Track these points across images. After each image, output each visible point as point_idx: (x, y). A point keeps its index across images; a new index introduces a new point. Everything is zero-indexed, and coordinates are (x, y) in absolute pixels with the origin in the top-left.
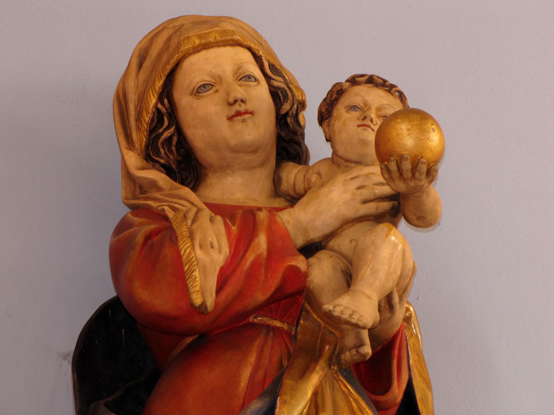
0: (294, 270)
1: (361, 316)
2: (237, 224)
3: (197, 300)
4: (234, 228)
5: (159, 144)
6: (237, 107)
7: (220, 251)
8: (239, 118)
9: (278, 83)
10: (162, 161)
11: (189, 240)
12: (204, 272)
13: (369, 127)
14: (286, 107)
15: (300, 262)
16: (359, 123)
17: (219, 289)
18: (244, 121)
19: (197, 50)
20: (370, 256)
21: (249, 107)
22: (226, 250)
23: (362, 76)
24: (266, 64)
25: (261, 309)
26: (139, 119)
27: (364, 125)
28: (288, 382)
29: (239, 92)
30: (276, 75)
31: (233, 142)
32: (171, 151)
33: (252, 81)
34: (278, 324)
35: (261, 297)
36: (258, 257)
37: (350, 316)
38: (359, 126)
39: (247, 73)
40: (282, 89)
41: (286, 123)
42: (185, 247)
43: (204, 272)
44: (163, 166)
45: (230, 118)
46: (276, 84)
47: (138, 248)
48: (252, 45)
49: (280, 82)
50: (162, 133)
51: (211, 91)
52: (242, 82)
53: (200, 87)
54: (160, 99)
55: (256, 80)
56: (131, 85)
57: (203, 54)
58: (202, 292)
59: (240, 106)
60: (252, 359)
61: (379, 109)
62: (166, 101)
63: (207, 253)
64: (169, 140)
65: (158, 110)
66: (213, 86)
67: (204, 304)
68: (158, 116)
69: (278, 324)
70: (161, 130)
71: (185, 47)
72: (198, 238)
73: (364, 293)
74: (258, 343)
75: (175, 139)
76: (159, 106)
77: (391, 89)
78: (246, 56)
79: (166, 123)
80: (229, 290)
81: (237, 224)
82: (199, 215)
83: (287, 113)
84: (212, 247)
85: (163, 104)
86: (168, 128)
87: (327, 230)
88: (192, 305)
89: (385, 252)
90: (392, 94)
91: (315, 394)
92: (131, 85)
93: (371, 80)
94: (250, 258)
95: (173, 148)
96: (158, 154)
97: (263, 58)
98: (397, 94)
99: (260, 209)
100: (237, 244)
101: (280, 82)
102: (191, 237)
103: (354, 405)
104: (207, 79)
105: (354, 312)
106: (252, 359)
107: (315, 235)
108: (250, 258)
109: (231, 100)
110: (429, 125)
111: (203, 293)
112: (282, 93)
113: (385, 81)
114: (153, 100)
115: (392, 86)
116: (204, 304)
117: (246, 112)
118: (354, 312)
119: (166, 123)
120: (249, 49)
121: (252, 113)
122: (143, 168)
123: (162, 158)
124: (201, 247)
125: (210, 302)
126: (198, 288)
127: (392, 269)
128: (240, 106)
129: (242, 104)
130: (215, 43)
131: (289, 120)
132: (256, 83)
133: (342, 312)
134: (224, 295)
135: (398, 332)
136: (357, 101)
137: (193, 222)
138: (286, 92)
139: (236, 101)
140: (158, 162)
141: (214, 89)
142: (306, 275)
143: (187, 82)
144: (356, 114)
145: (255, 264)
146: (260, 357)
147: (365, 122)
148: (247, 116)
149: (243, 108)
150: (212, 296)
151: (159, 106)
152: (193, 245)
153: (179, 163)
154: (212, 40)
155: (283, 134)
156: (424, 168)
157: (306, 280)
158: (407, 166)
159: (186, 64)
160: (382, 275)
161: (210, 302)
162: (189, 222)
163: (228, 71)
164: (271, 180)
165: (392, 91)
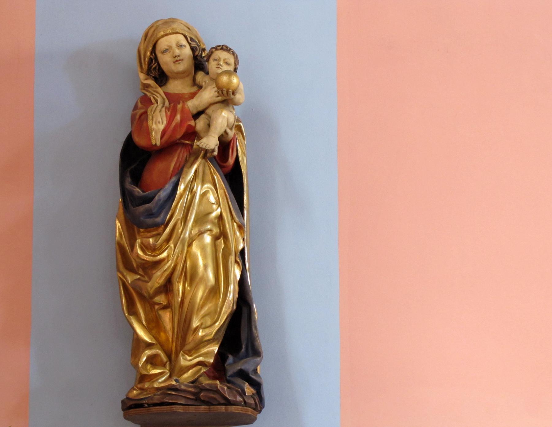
1: (210, 146)
2: (170, 111)
3: (154, 143)
4: (169, 113)
5: (152, 70)
6: (176, 59)
7: (162, 123)
8: (177, 62)
9: (194, 44)
10: (153, 75)
11: (152, 120)
12: (156, 132)
13: (220, 68)
14: (197, 53)
15: (192, 123)
16: (217, 66)
17: (162, 138)
18: (179, 63)
19: (163, 36)
20: (214, 122)
21: (181, 58)
22: (165, 122)
24: (189, 39)
26: (144, 60)
27: (218, 67)
28: (185, 169)
29: (177, 52)
30: (193, 42)
31: (175, 71)
32: (156, 72)
33: (183, 47)
34: (187, 142)
35: (178, 137)
36: (177, 124)
37: (205, 147)
38: (216, 68)
39: (181, 44)
40: (195, 47)
41: (197, 58)
42: (150, 122)
43: (156, 132)
44: (153, 77)
45: (174, 62)
46: (192, 45)
47: (136, 121)
48: (183, 33)
49: (194, 44)
50: (152, 66)
51: (168, 52)
52: (179, 48)
53: (164, 51)
54: (151, 54)
55: (185, 46)
56: (142, 48)
57: (165, 38)
58: (155, 139)
59: (178, 58)
60: (175, 159)
61: (224, 60)
62: (153, 54)
63: (157, 126)
64: (155, 68)
65: (151, 58)
66: (168, 50)
67: (156, 144)
68: (151, 60)
69: (187, 142)
70: (152, 65)
72: (154, 119)
73: (212, 136)
74: (178, 151)
75: (157, 68)
76: (151, 56)
77: (229, 51)
78: (181, 37)
79: (154, 62)
80: (166, 137)
81: (170, 111)
82: (156, 109)
83: (197, 55)
84: (159, 123)
85: (152, 55)
86: (155, 64)
87: (204, 107)
88: (152, 144)
89: (220, 120)
90: (230, 53)
91: (196, 171)
92: (142, 48)
94: (174, 124)
95: (157, 71)
96: (152, 73)
97: (188, 37)
98: (232, 53)
100: (169, 119)
101: (194, 44)
102: (152, 119)
103: (212, 170)
104: (166, 47)
105: (207, 144)
106: (175, 159)
107: (200, 109)
108: (174, 124)
109: (174, 56)
110: (232, 77)
111: (155, 140)
112: (195, 48)
114: (148, 54)
115: (230, 49)
116: (156, 144)
117: (180, 60)
118: (207, 144)
119: (154, 62)
120: (182, 34)
121: (182, 60)
122: (146, 79)
123: (153, 74)
124: (155, 123)
125: (158, 144)
126: (154, 139)
127: (222, 126)
128: (178, 58)
129: (178, 57)
131: (198, 57)
132: (184, 47)
133: (203, 145)
134: (164, 139)
135: (232, 139)
136: (217, 57)
137: (154, 113)
138: (197, 48)
141: (169, 51)
142: (195, 127)
143: (159, 49)
144: (216, 63)
145: (175, 127)
146: (178, 158)
147: (218, 66)
148: (180, 61)
149: (179, 58)
150: (159, 141)
151: (151, 56)
152: (152, 123)
153: (159, 75)
154: (168, 33)
155: (196, 62)
158: (225, 92)
159: (159, 42)
160: (218, 129)
161: (158, 144)
162: (152, 113)
164: (192, 79)
165: (230, 52)
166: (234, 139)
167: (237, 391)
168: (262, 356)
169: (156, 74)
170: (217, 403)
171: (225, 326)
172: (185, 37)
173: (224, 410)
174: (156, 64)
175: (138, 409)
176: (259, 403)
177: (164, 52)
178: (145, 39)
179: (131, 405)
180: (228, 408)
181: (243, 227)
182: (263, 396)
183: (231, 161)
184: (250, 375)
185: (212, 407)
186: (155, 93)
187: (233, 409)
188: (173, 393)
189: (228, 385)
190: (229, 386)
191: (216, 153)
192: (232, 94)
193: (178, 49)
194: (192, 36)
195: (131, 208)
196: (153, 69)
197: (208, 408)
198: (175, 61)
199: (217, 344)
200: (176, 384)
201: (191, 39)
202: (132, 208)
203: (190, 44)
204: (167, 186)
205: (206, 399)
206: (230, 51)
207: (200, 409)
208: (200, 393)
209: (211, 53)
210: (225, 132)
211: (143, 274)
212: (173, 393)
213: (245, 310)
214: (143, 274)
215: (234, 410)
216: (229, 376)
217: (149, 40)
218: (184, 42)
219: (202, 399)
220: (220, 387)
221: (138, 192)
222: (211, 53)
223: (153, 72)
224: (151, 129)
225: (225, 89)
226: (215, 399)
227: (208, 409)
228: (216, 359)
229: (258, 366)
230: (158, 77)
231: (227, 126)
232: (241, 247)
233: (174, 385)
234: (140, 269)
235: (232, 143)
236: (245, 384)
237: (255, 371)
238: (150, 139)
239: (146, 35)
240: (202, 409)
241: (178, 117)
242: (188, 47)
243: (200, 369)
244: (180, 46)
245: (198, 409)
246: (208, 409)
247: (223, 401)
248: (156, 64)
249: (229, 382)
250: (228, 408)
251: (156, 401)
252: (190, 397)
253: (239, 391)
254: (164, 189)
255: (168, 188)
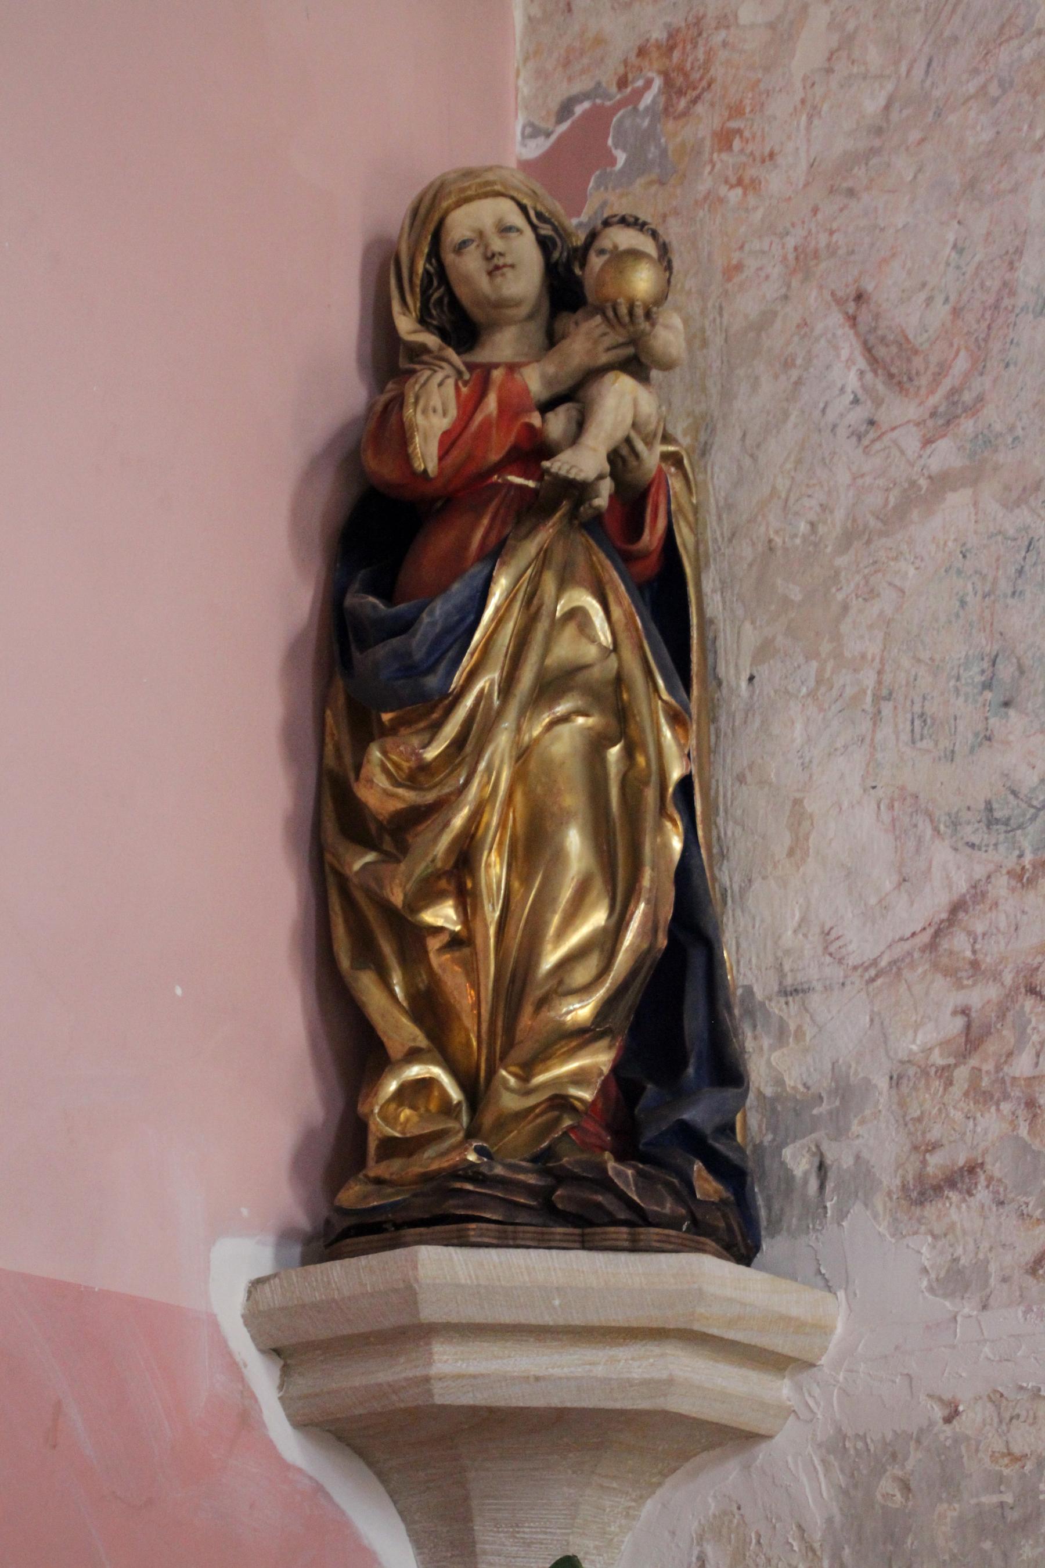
0: (530, 427)
3: (419, 465)
4: (464, 390)
9: (546, 230)
10: (435, 323)
12: (425, 438)
15: (536, 419)
17: (441, 459)
19: (458, 204)
21: (508, 260)
22: (453, 412)
23: (615, 216)
24: (532, 214)
25: (500, 467)
26: (411, 281)
40: (550, 238)
42: (409, 412)
43: (425, 438)
46: (543, 232)
48: (515, 194)
50: (432, 295)
55: (519, 230)
57: (465, 209)
62: (434, 261)
64: (440, 300)
67: (425, 471)
70: (431, 291)
71: (445, 204)
75: (446, 300)
79: (435, 283)
80: (456, 455)
84: (435, 411)
85: (431, 264)
86: (438, 288)
93: (624, 221)
95: (445, 309)
96: (431, 316)
99: (496, 366)
102: (416, 403)
108: (479, 418)
109: (489, 254)
113: (637, 219)
115: (644, 224)
116: (425, 471)
117: (505, 266)
119: (435, 283)
120: (513, 198)
121: (512, 266)
122: (415, 332)
130: (476, 196)
134: (449, 460)
135: (650, 485)
139: (493, 255)
140: (431, 324)
151: (428, 266)
156: (640, 312)
157: (406, 451)
158: (623, 310)
163: (488, 223)
166: (659, 484)
167: (669, 1185)
168: (745, 1084)
169: (444, 317)
170: (606, 1220)
171: (631, 997)
172: (523, 209)
173: (627, 1240)
174: (442, 290)
175: (363, 1239)
176: (740, 1229)
177: (461, 246)
178: (412, 225)
179: (349, 1228)
180: (639, 1234)
181: (687, 717)
182: (578, 922)
183: (651, 538)
184: (710, 1141)
185: (588, 1230)
186: (437, 362)
187: (656, 1238)
188: (470, 1187)
189: (641, 1166)
190: (642, 1170)
191: (602, 501)
192: (642, 318)
193: (502, 238)
194: (540, 208)
195: (357, 655)
196: (435, 305)
197: (579, 1235)
198: (491, 267)
199: (610, 1047)
200: (478, 1162)
201: (539, 215)
202: (358, 654)
203: (534, 228)
204: (456, 587)
205: (571, 1208)
206: (646, 227)
207: (551, 1237)
208: (553, 1190)
209: (593, 236)
210: (628, 441)
211: (394, 851)
212: (470, 1187)
213: (697, 960)
214: (394, 851)
215: (655, 1241)
216: (646, 1144)
217: (424, 223)
218: (516, 219)
219: (560, 1206)
220: (614, 1168)
221: (374, 607)
222: (593, 236)
223: (434, 312)
224: (411, 426)
225: (621, 300)
226: (599, 1206)
227: (577, 1238)
228: (603, 1091)
229: (737, 1113)
230: (448, 327)
231: (634, 425)
232: (676, 774)
233: (472, 1164)
234: (387, 838)
235: (653, 490)
236: (692, 1164)
237: (727, 1129)
238: (407, 459)
239: (415, 212)
240: (558, 1237)
241: (491, 403)
242: (529, 234)
243: (557, 1121)
244: (505, 230)
245: (546, 1237)
246: (577, 1238)
247: (622, 1216)
248: (442, 290)
249: (645, 1159)
250: (639, 1234)
251: (416, 1214)
252: (522, 1201)
253: (673, 1183)
254: (448, 592)
255: (459, 592)
